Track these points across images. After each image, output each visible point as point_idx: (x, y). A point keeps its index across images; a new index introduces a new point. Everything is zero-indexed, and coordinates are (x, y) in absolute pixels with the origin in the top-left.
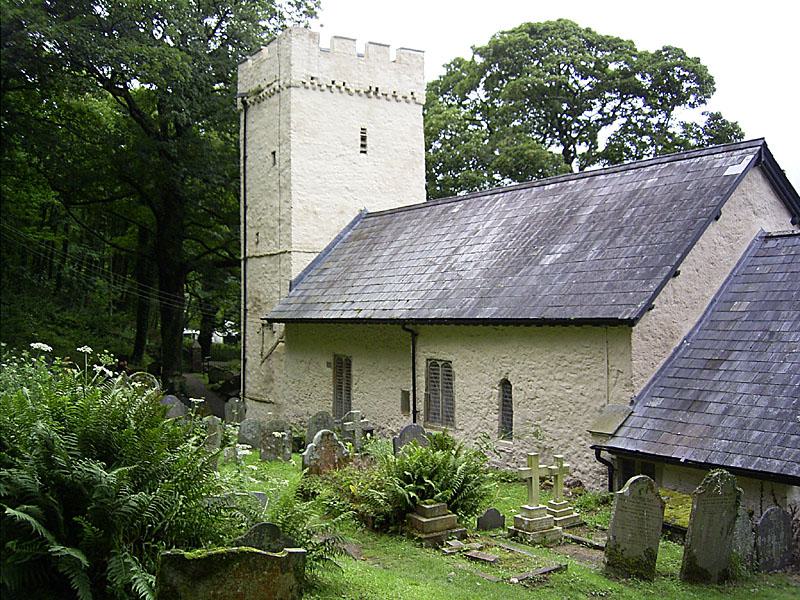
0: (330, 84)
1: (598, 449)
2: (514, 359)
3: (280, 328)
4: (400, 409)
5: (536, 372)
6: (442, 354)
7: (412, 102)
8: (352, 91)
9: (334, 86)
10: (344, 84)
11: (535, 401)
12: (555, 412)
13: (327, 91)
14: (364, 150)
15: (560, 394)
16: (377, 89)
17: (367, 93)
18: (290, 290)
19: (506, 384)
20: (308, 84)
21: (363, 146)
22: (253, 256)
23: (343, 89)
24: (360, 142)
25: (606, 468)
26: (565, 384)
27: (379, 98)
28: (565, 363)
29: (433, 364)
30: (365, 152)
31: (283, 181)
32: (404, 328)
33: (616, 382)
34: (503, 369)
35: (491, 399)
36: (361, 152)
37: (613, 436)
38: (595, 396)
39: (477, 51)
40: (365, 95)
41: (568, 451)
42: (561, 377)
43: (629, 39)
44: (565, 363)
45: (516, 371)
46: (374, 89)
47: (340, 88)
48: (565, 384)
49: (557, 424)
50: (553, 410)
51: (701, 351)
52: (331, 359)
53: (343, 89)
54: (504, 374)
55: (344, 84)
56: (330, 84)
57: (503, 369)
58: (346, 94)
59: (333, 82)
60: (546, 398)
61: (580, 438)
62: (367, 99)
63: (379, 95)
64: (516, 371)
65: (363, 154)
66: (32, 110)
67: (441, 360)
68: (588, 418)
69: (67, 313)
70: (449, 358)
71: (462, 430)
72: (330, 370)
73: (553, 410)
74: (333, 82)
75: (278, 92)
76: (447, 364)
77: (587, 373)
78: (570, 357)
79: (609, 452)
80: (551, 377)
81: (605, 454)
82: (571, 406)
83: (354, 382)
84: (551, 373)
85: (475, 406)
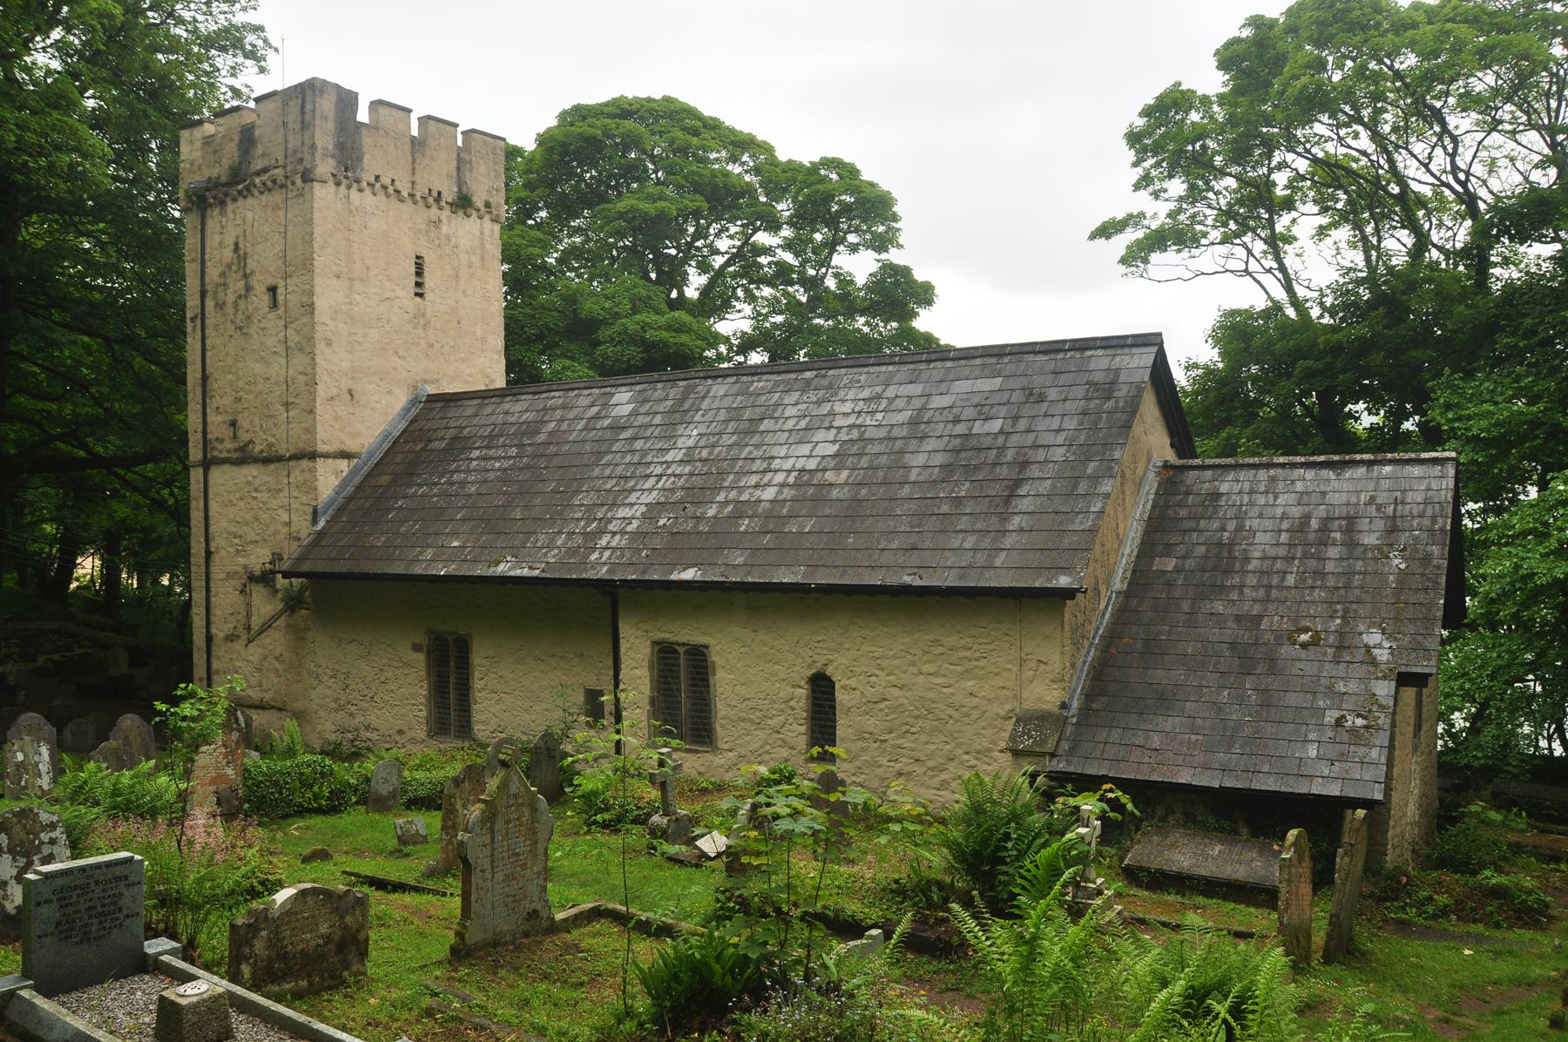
2: (840, 644)
5: (885, 663)
6: (686, 633)
8: (405, 193)
9: (378, 185)
10: (393, 181)
11: (881, 706)
13: (368, 191)
15: (932, 695)
16: (439, 193)
19: (821, 688)
21: (418, 284)
23: (391, 190)
24: (413, 279)
28: (941, 650)
29: (665, 654)
31: (294, 337)
33: (1035, 676)
34: (816, 658)
35: (792, 703)
39: (1136, 164)
41: (944, 776)
43: (1123, 144)
44: (941, 650)
46: (435, 194)
49: (923, 738)
50: (916, 718)
52: (421, 639)
53: (391, 190)
55: (393, 181)
56: (373, 180)
58: (393, 200)
59: (377, 178)
60: (902, 701)
61: (967, 757)
63: (443, 204)
64: (844, 661)
65: (418, 299)
67: (684, 644)
68: (983, 728)
69: (313, 943)
70: (697, 638)
72: (420, 658)
73: (916, 718)
74: (377, 178)
77: (983, 663)
78: (952, 640)
82: (951, 711)
83: (477, 675)
84: (913, 664)
85: (759, 714)
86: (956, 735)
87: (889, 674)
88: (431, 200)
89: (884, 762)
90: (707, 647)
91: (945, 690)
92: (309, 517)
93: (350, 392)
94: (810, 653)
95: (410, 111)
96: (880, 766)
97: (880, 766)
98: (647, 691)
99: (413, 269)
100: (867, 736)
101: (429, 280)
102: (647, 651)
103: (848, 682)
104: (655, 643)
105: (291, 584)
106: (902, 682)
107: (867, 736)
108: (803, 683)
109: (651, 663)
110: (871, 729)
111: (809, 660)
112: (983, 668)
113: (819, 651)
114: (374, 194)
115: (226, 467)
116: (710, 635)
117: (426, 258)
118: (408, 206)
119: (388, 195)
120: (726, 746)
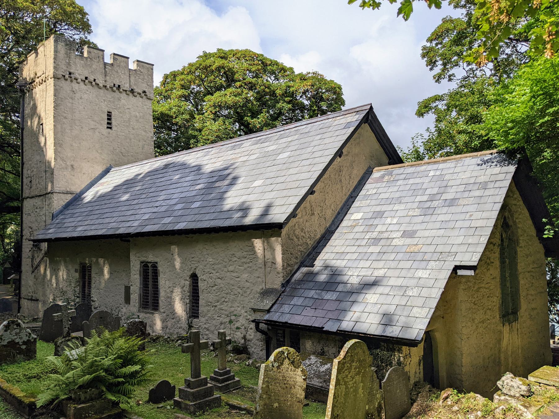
0: (84, 79)
1: (257, 323)
3: (45, 246)
4: (123, 300)
5: (215, 267)
6: (151, 258)
7: (145, 97)
8: (101, 85)
9: (87, 81)
11: (214, 288)
12: (228, 295)
13: (82, 83)
14: (109, 121)
15: (232, 282)
17: (111, 88)
18: (52, 220)
20: (67, 76)
21: (108, 123)
22: (28, 197)
23: (94, 83)
24: (106, 121)
25: (263, 336)
26: (235, 274)
27: (121, 92)
30: (111, 128)
32: (122, 240)
33: (271, 271)
34: (192, 266)
36: (108, 128)
37: (268, 311)
38: (256, 282)
40: (110, 89)
42: (232, 270)
45: (201, 267)
46: (117, 86)
47: (92, 83)
48: (235, 274)
50: (227, 294)
51: (258, 162)
52: (77, 267)
53: (94, 83)
54: (193, 269)
56: (84, 79)
57: (192, 266)
58: (96, 87)
62: (111, 93)
63: (121, 90)
64: (201, 267)
65: (109, 130)
66: (11, 246)
71: (164, 312)
73: (227, 294)
75: (45, 81)
76: (155, 266)
77: (251, 265)
79: (265, 324)
80: (226, 269)
81: (262, 326)
82: (239, 290)
86: (241, 302)
87: (217, 273)
88: (115, 89)
89: (216, 317)
90: (157, 263)
91: (237, 279)
92: (51, 218)
93: (72, 166)
94: (190, 263)
95: (128, 58)
96: (214, 319)
97: (214, 319)
98: (138, 285)
99: (106, 117)
100: (210, 304)
101: (113, 121)
102: (139, 266)
103: (203, 277)
104: (142, 262)
105: (12, 228)
106: (221, 276)
107: (210, 304)
108: (188, 278)
109: (140, 271)
110: (211, 300)
111: (190, 267)
112: (251, 267)
113: (193, 262)
114: (86, 85)
115: (28, 199)
116: (157, 257)
117: (113, 113)
118: (102, 91)
119: (92, 85)
120: (119, 287)
